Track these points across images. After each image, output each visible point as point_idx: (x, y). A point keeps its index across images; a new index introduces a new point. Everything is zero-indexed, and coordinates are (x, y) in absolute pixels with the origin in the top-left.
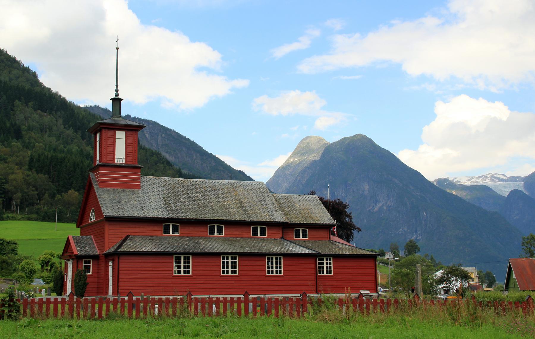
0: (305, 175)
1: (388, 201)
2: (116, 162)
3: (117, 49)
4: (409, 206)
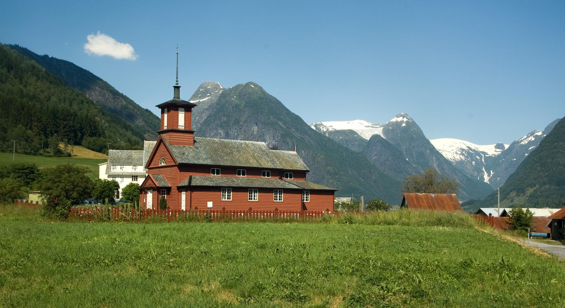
0: (203, 116)
1: (273, 140)
2: (179, 128)
4: (291, 145)
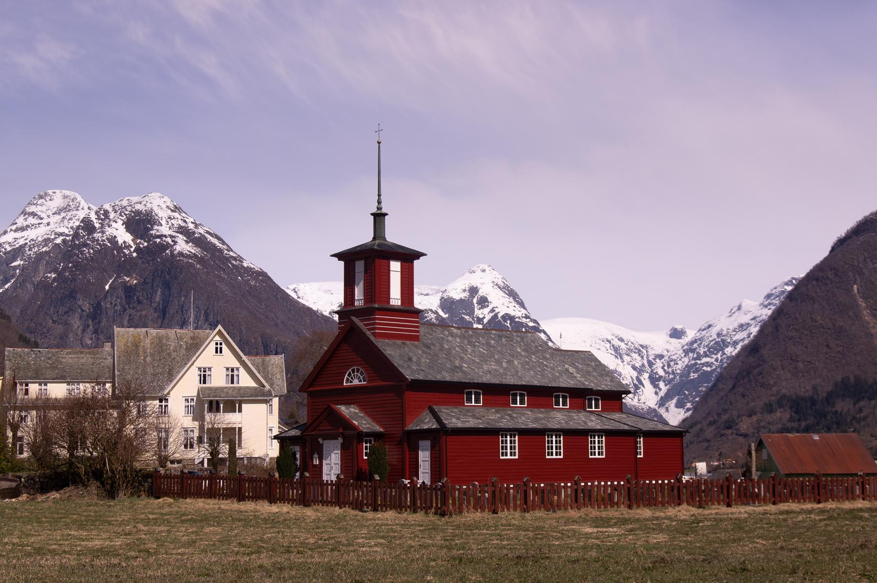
2: (391, 304)
3: (379, 143)
